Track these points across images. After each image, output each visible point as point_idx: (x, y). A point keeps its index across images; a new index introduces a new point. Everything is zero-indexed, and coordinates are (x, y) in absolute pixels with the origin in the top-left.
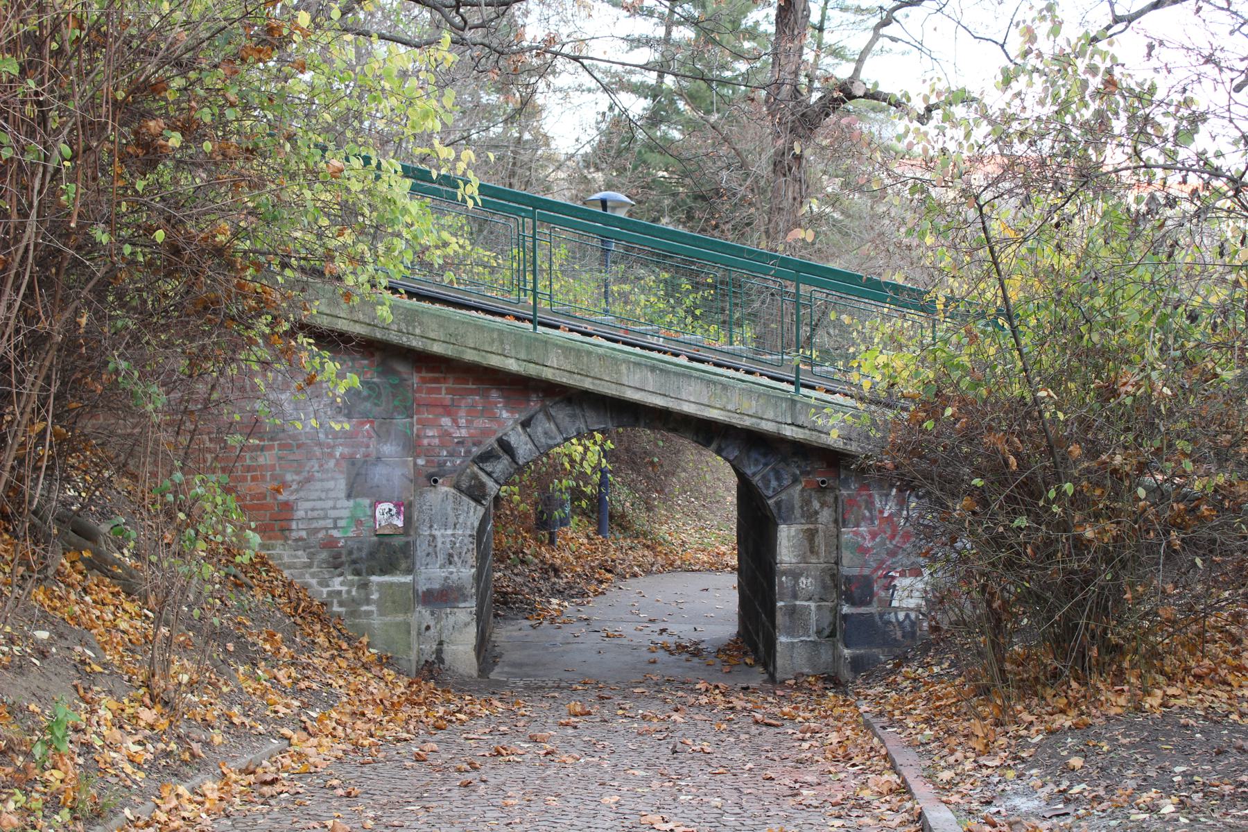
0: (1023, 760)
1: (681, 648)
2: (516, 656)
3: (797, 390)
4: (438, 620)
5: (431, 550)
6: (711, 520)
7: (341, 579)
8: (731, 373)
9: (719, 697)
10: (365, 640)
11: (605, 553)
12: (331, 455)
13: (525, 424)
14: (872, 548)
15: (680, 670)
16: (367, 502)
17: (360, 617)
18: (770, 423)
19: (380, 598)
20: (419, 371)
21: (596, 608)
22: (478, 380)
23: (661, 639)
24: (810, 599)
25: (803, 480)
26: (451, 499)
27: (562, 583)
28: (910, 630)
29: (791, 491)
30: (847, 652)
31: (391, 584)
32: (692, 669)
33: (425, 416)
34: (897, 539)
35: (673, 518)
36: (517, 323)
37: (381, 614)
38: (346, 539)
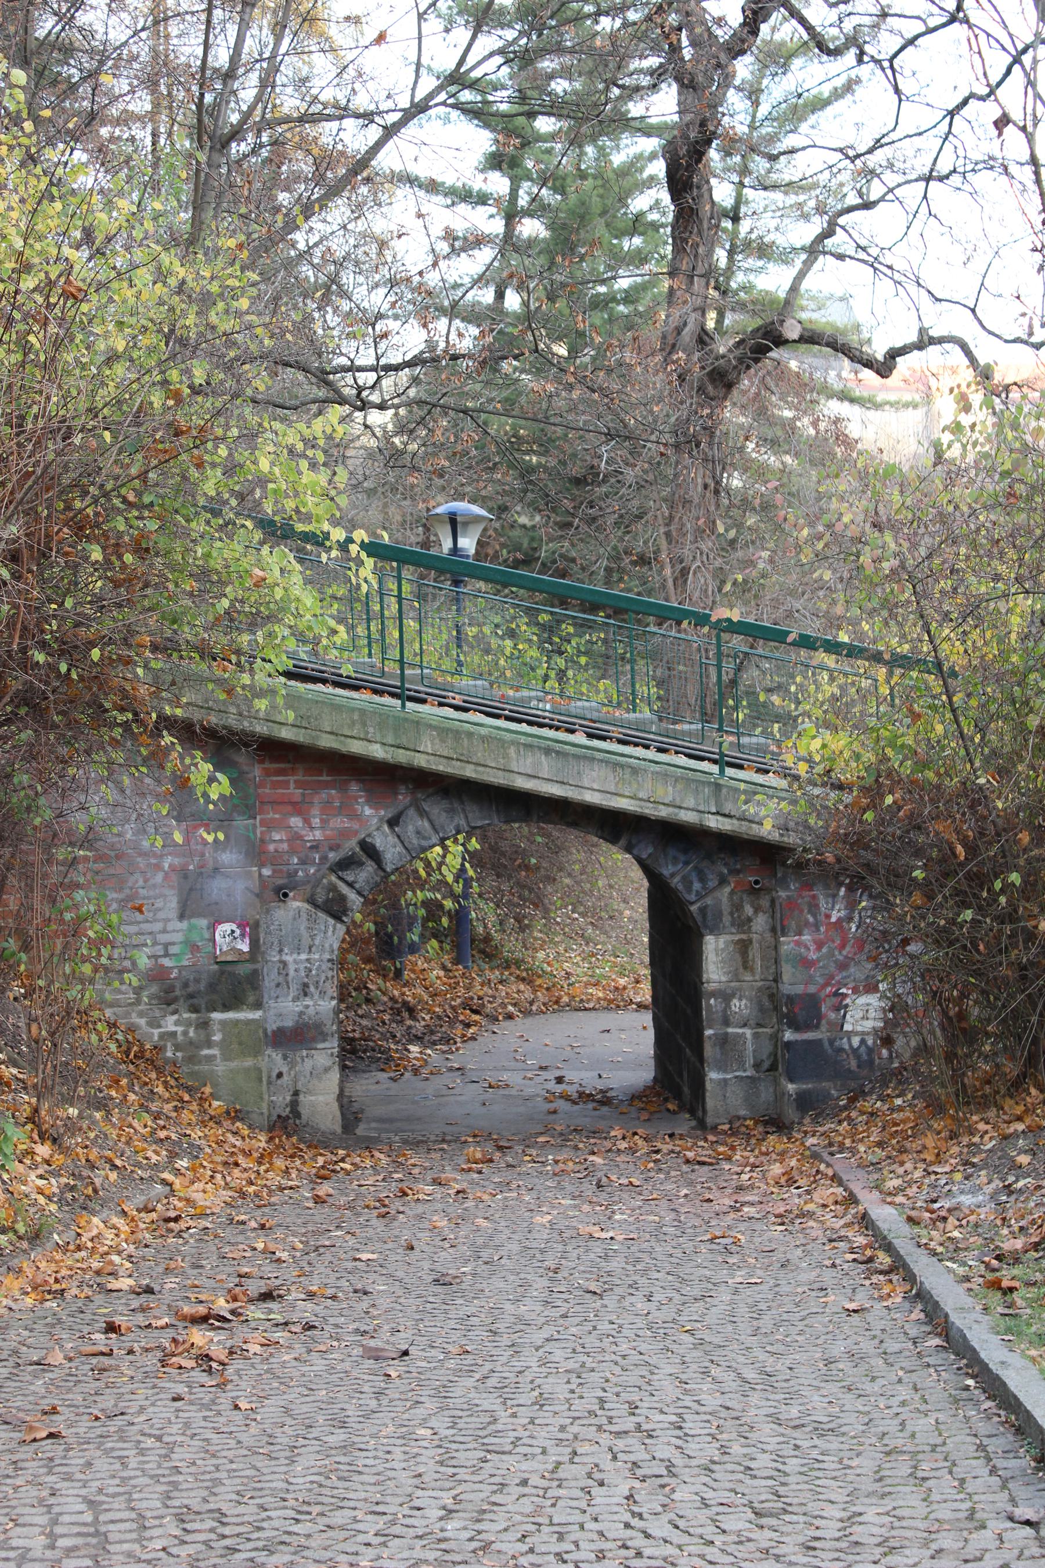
0: (974, 1165)
1: (584, 1097)
2: (380, 1111)
3: (722, 772)
4: (292, 1065)
5: (281, 979)
6: (604, 943)
7: (175, 1017)
8: (640, 752)
9: (640, 1142)
10: (208, 1090)
11: (468, 988)
12: (158, 867)
13: (393, 822)
14: (818, 960)
15: (588, 1120)
16: (203, 922)
17: (200, 1062)
18: (690, 813)
19: (223, 1040)
20: (261, 762)
21: (466, 1055)
22: (334, 771)
23: (559, 1089)
24: (745, 1025)
25: (732, 880)
26: (304, 916)
27: (419, 1027)
28: (867, 1060)
29: (717, 894)
30: (791, 1087)
31: (237, 1022)
32: (602, 1118)
33: (271, 815)
34: (848, 949)
35: (551, 941)
36: (377, 698)
37: (226, 1058)
38: (181, 968)
